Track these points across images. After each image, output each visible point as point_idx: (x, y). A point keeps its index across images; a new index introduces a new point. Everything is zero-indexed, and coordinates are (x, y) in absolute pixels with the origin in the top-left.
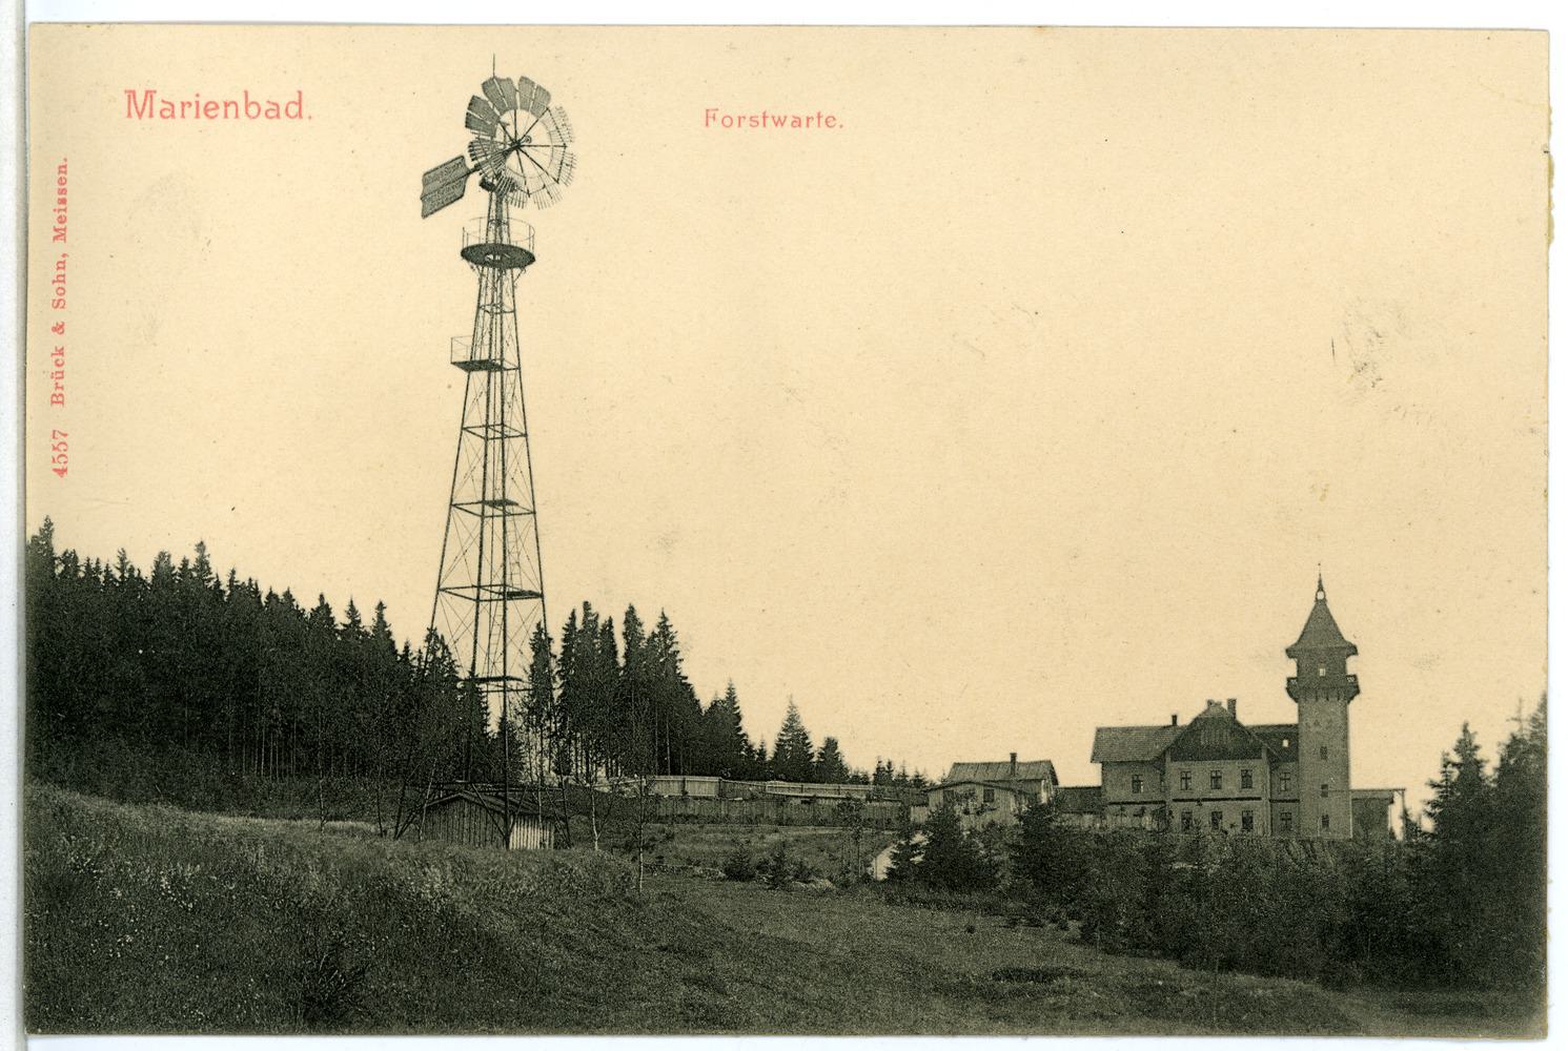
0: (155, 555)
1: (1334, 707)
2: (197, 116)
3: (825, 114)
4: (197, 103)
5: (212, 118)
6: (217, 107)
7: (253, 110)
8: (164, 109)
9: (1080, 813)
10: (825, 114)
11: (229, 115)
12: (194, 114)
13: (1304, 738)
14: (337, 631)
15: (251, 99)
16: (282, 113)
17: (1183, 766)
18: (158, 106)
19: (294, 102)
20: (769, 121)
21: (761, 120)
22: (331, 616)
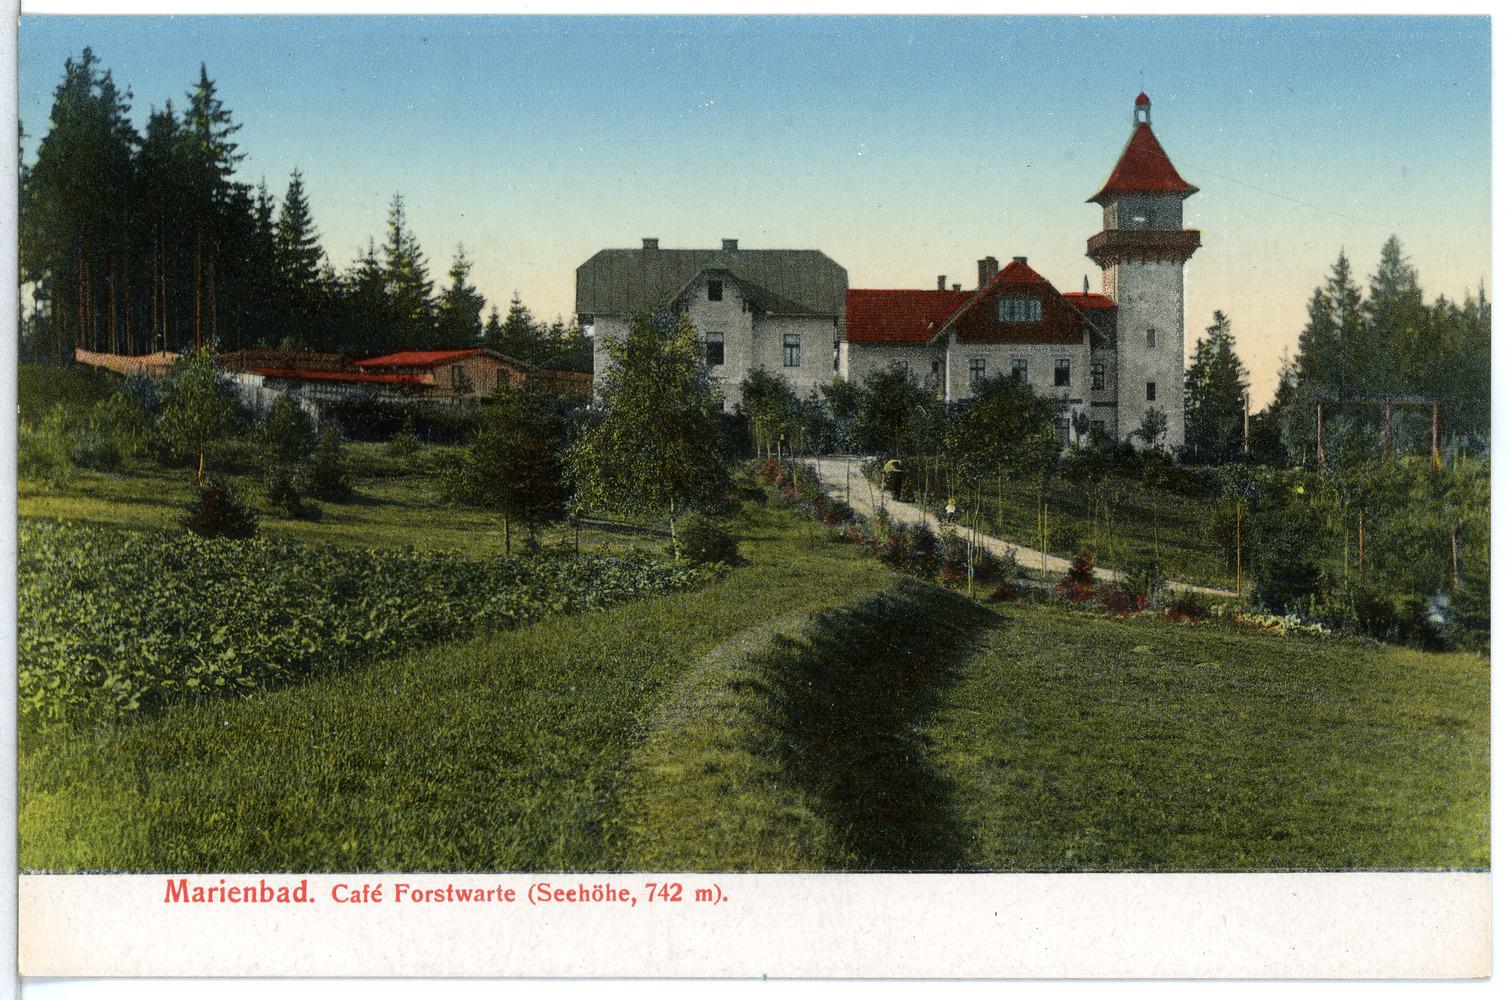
0: (1385, 240)
1: (1166, 269)
2: (222, 900)
3: (504, 889)
4: (223, 890)
5: (511, 900)
6: (239, 892)
7: (267, 894)
8: (195, 895)
9: (460, 356)
10: (504, 889)
11: (213, 898)
12: (219, 898)
13: (1125, 316)
14: (256, 220)
15: (265, 887)
16: (424, 894)
17: (973, 349)
18: (191, 894)
19: (299, 888)
20: (454, 895)
21: (446, 895)
22: (970, 282)
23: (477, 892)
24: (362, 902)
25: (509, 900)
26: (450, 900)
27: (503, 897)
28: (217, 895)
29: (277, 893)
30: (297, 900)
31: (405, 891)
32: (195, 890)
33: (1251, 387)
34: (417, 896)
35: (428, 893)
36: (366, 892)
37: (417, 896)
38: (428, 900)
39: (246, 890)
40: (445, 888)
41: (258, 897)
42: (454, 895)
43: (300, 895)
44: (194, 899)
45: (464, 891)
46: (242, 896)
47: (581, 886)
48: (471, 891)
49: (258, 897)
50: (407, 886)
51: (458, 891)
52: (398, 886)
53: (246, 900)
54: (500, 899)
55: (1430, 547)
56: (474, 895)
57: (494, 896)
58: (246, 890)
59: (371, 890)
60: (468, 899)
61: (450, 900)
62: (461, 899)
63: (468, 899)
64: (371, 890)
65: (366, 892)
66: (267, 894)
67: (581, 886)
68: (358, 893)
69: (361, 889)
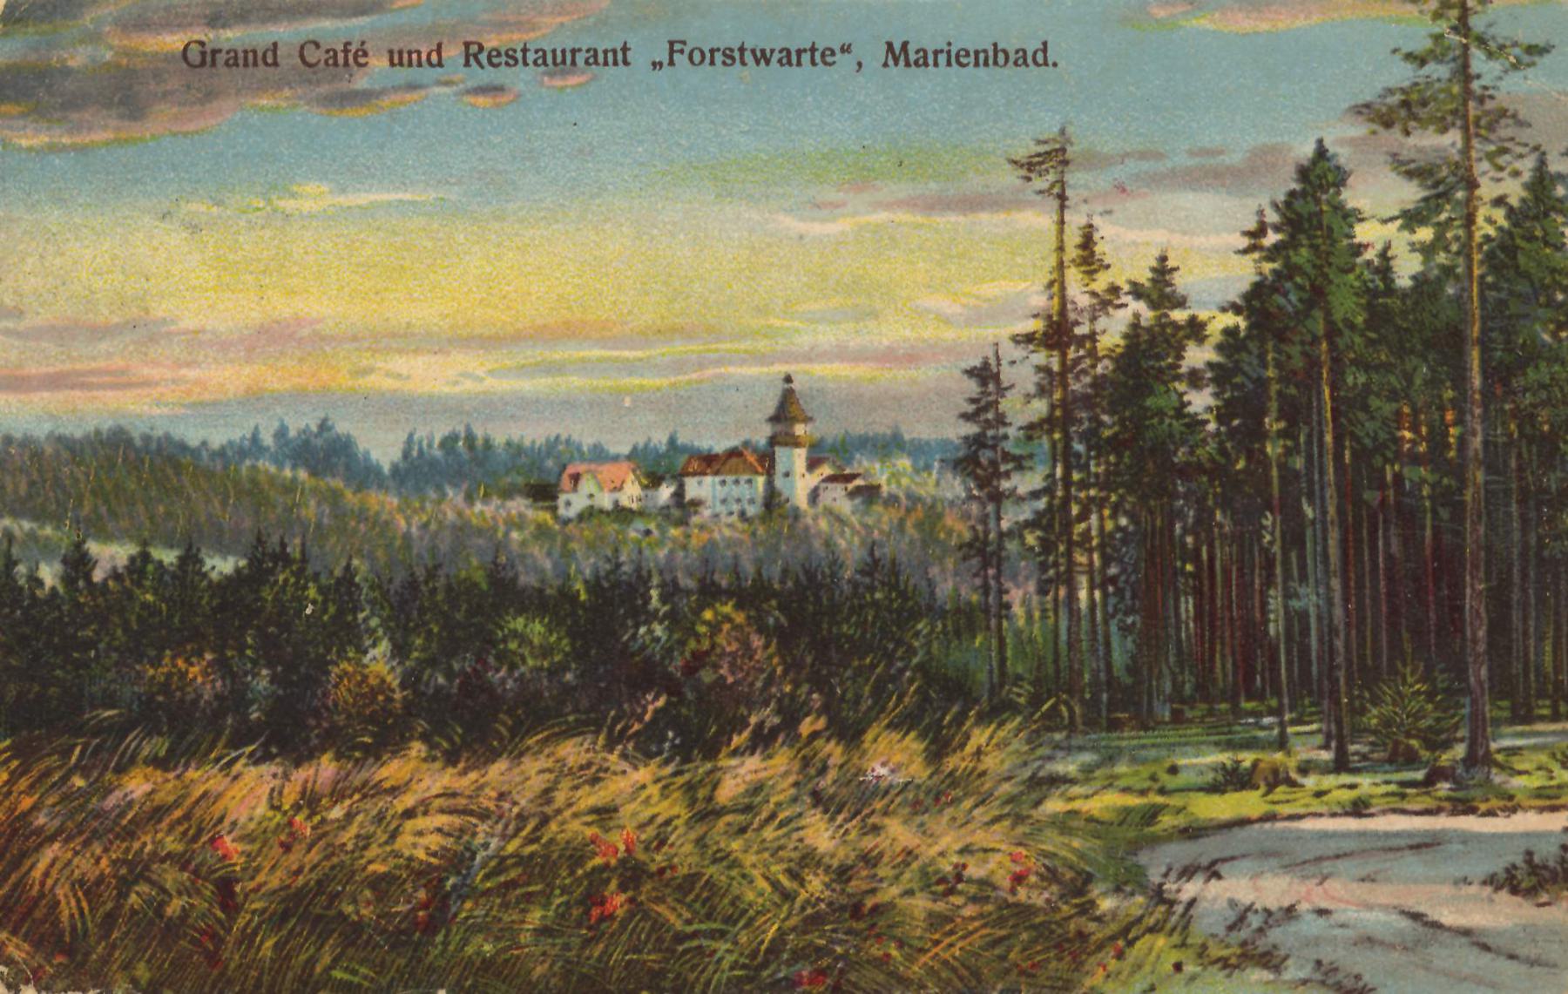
2: (949, 64)
4: (949, 52)
7: (1001, 57)
16: (260, 62)
18: (912, 57)
20: (748, 57)
23: (781, 51)
24: (931, 68)
25: (826, 63)
26: (743, 63)
27: (351, 60)
28: (942, 59)
29: (1012, 57)
30: (266, 64)
31: (682, 51)
32: (917, 52)
33: (1394, 245)
34: (697, 57)
35: (712, 51)
36: (346, 51)
37: (697, 57)
38: (712, 63)
39: (977, 53)
40: (519, 47)
41: (991, 61)
42: (748, 57)
43: (434, 58)
44: (916, 63)
45: (763, 51)
46: (972, 59)
47: (995, 45)
48: (772, 51)
49: (991, 61)
50: (684, 43)
51: (753, 51)
52: (672, 43)
53: (977, 64)
54: (813, 63)
55: (1101, 507)
56: (776, 56)
57: (806, 58)
58: (977, 53)
59: (353, 48)
60: (768, 62)
61: (743, 63)
62: (758, 62)
63: (768, 62)
64: (353, 48)
65: (346, 51)
66: (1001, 57)
67: (995, 45)
68: (335, 53)
69: (340, 47)
